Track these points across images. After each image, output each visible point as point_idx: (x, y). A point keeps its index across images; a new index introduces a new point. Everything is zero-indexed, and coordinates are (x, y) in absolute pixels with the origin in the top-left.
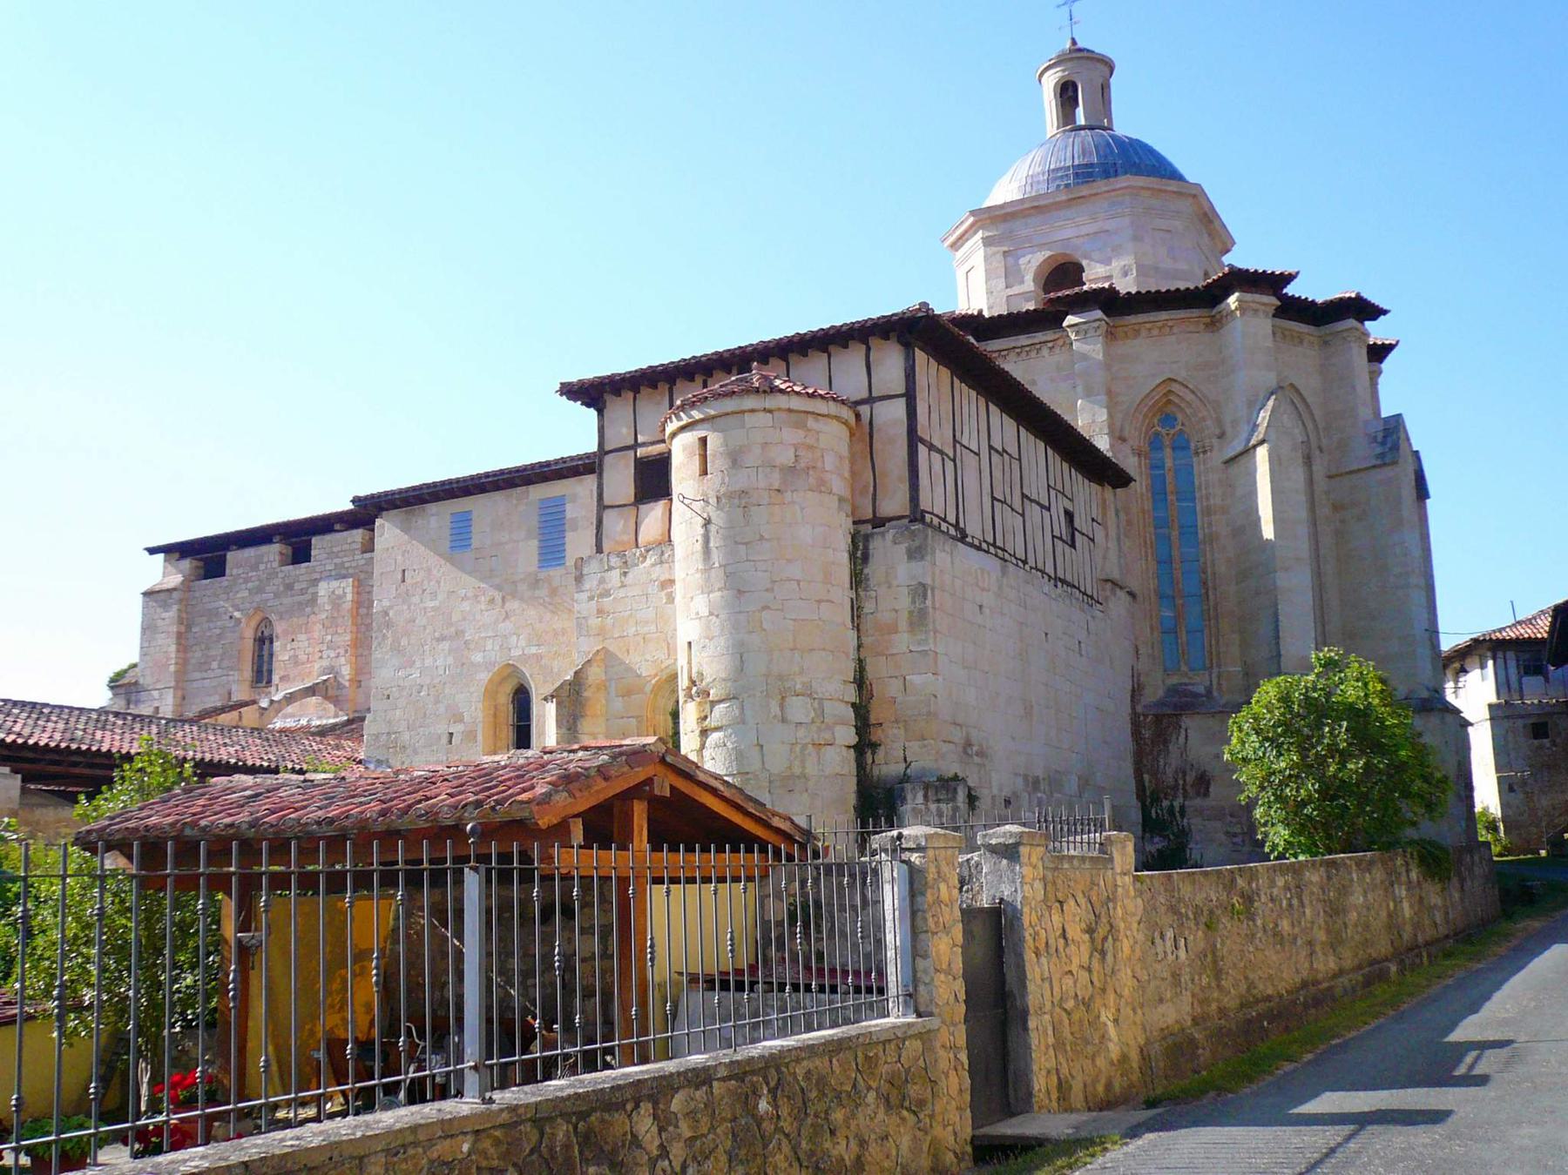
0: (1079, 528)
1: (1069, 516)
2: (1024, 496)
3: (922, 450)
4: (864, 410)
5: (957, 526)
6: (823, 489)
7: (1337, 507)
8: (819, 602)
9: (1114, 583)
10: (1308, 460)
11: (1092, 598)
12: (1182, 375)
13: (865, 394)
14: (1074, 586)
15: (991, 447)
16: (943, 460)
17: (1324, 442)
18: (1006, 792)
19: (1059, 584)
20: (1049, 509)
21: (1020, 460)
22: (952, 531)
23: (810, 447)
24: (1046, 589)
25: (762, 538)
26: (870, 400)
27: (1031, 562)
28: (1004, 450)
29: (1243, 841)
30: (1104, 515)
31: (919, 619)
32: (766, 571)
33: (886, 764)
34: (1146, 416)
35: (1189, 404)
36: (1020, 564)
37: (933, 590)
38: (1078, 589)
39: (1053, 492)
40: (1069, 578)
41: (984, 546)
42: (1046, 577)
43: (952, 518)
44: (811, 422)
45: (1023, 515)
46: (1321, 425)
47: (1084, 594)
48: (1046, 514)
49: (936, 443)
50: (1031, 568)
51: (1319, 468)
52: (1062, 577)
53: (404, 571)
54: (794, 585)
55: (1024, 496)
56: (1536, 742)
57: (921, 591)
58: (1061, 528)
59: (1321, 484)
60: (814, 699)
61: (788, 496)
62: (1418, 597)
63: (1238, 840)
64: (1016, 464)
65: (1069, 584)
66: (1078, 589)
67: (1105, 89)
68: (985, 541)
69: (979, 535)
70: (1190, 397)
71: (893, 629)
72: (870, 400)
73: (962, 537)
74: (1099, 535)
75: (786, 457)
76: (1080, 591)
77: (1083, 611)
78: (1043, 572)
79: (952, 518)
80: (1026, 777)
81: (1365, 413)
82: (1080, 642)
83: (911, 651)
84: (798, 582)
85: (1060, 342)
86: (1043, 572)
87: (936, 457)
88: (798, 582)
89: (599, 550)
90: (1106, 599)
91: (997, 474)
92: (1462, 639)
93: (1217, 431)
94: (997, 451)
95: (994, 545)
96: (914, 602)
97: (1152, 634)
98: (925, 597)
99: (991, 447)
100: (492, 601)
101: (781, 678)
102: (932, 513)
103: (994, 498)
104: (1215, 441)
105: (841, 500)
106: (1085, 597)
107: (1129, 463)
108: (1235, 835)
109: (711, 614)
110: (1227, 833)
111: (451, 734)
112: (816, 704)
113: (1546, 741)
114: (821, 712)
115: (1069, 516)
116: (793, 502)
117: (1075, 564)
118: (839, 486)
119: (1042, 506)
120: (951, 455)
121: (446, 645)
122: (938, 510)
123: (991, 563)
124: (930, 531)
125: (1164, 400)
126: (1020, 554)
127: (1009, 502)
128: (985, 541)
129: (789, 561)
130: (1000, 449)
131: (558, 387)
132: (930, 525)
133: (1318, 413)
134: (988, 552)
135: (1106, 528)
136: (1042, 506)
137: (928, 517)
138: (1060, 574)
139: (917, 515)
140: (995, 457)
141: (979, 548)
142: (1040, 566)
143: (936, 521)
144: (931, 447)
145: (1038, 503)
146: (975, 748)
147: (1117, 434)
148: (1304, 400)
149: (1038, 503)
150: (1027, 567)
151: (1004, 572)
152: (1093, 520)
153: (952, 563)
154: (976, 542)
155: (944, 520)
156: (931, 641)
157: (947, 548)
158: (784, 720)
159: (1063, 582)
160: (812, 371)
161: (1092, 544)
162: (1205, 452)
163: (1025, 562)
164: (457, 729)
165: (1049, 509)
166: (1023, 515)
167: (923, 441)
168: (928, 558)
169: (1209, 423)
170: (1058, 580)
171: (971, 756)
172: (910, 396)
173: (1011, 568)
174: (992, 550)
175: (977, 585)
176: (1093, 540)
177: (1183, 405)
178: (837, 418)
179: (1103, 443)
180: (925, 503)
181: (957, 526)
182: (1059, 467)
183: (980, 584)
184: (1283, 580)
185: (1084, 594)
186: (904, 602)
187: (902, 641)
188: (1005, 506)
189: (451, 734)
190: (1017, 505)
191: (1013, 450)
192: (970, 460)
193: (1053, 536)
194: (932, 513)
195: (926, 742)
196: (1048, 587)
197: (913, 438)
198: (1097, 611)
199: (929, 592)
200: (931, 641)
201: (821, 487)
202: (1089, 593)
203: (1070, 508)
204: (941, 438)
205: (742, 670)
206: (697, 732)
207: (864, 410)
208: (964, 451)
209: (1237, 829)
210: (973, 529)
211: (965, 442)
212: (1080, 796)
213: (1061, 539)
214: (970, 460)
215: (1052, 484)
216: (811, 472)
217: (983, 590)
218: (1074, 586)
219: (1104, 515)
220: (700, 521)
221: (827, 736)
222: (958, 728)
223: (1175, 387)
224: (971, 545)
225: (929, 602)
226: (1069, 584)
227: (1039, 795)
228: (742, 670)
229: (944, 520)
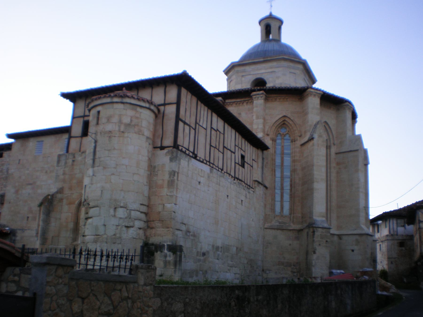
0: (247, 161)
1: (243, 157)
2: (224, 147)
3: (181, 124)
4: (162, 108)
5: (193, 153)
6: (140, 133)
7: (338, 164)
8: (134, 174)
9: (259, 182)
10: (328, 147)
11: (250, 186)
12: (289, 115)
13: (163, 102)
14: (243, 181)
15: (212, 128)
16: (190, 128)
17: (335, 142)
18: (204, 250)
19: (236, 180)
20: (234, 153)
21: (224, 134)
22: (191, 154)
23: (137, 118)
24: (229, 180)
25: (114, 149)
26: (164, 105)
27: (225, 170)
28: (218, 130)
29: (297, 275)
30: (258, 158)
31: (171, 184)
32: (115, 161)
33: (154, 236)
34: (276, 127)
35: (291, 125)
36: (220, 170)
37: (178, 173)
38: (244, 182)
39: (237, 148)
40: (240, 178)
41: (205, 162)
42: (231, 176)
43: (191, 149)
44: (139, 109)
45: (223, 153)
46: (335, 136)
47: (247, 184)
48: (233, 155)
49: (187, 121)
50: (225, 172)
51: (334, 150)
52: (237, 177)
53: (19, 163)
54: (124, 167)
55: (224, 147)
56: (401, 248)
57: (173, 173)
58: (239, 160)
59: (333, 155)
60: (128, 209)
61: (126, 135)
62: (362, 196)
63: (295, 274)
64: (222, 136)
65: (240, 180)
66: (244, 182)
67: (280, 28)
68: (205, 160)
69: (203, 158)
70: (291, 122)
71: (162, 187)
72: (164, 105)
73: (195, 157)
74: (255, 165)
75: (127, 120)
76: (245, 183)
77: (245, 190)
78: (230, 175)
79: (191, 149)
80: (213, 246)
81: (349, 133)
82: (242, 201)
83: (167, 195)
84: (126, 166)
85: (250, 101)
86: (230, 175)
87: (187, 128)
88: (126, 166)
89: (67, 151)
90: (255, 187)
91: (213, 138)
92: (379, 212)
93: (299, 134)
94: (214, 129)
95: (209, 162)
96: (170, 177)
97: (272, 201)
98: (174, 175)
99: (212, 128)
100: (46, 172)
101: (115, 200)
102: (183, 147)
103: (211, 146)
104: (298, 138)
105: (148, 138)
106: (247, 186)
107: (268, 142)
108: (294, 272)
109: (93, 175)
110: (292, 271)
111: (28, 217)
112: (128, 211)
113: (403, 248)
114: (130, 214)
115: (243, 157)
116: (128, 137)
117: (241, 172)
118: (147, 133)
119: (232, 152)
120: (194, 127)
121: (30, 187)
122: (186, 145)
123: (206, 168)
124: (179, 152)
125: (282, 123)
126: (220, 166)
127: (217, 148)
128: (205, 160)
129: (124, 158)
130: (216, 129)
131: (60, 93)
132: (181, 151)
133: (334, 133)
134: (206, 164)
135: (258, 163)
136: (232, 152)
137: (180, 148)
138: (237, 176)
139: (176, 146)
140: (213, 132)
141: (202, 162)
142: (229, 172)
143: (184, 150)
144: (185, 123)
145: (230, 150)
146: (191, 233)
147: (266, 133)
148: (329, 127)
149: (230, 150)
150: (223, 172)
151: (211, 171)
152: (253, 160)
153: (188, 165)
154: (201, 160)
155: (188, 150)
156: (175, 192)
157: (187, 159)
158: (114, 216)
159: (238, 179)
160: (145, 94)
161: (251, 168)
162: (295, 141)
163: (222, 170)
164: (30, 215)
165: (234, 153)
166: (223, 153)
167: (182, 121)
168: (177, 161)
169: (297, 131)
170: (235, 178)
171: (189, 236)
172: (178, 104)
173: (215, 170)
174: (208, 163)
175: (199, 174)
176: (252, 167)
177: (289, 125)
178: (149, 109)
179: (260, 135)
180: (180, 142)
181: (193, 153)
182: (240, 140)
183: (200, 174)
184: (316, 185)
185: (247, 184)
186: (167, 177)
187: (165, 191)
188: (216, 149)
189: (28, 217)
190: (221, 149)
191: (222, 131)
192: (202, 131)
193: (235, 163)
194: (183, 147)
195: (169, 229)
196: (230, 180)
197: (178, 119)
198: (251, 191)
199: (176, 174)
200: (175, 192)
201: (140, 133)
202: (249, 184)
203: (243, 154)
204: (191, 121)
205: (101, 196)
206: (84, 219)
207: (162, 108)
208: (200, 127)
209: (295, 270)
210: (201, 154)
211: (201, 124)
212: (237, 254)
213: (238, 164)
214: (202, 131)
215: (237, 144)
216: (136, 127)
217: (201, 176)
218: (243, 181)
219: (258, 158)
220: (93, 141)
221: (131, 224)
222: (184, 225)
223: (287, 119)
224: (199, 161)
225: (176, 178)
226: (240, 180)
227: (219, 253)
228: (101, 196)
229: (188, 150)
